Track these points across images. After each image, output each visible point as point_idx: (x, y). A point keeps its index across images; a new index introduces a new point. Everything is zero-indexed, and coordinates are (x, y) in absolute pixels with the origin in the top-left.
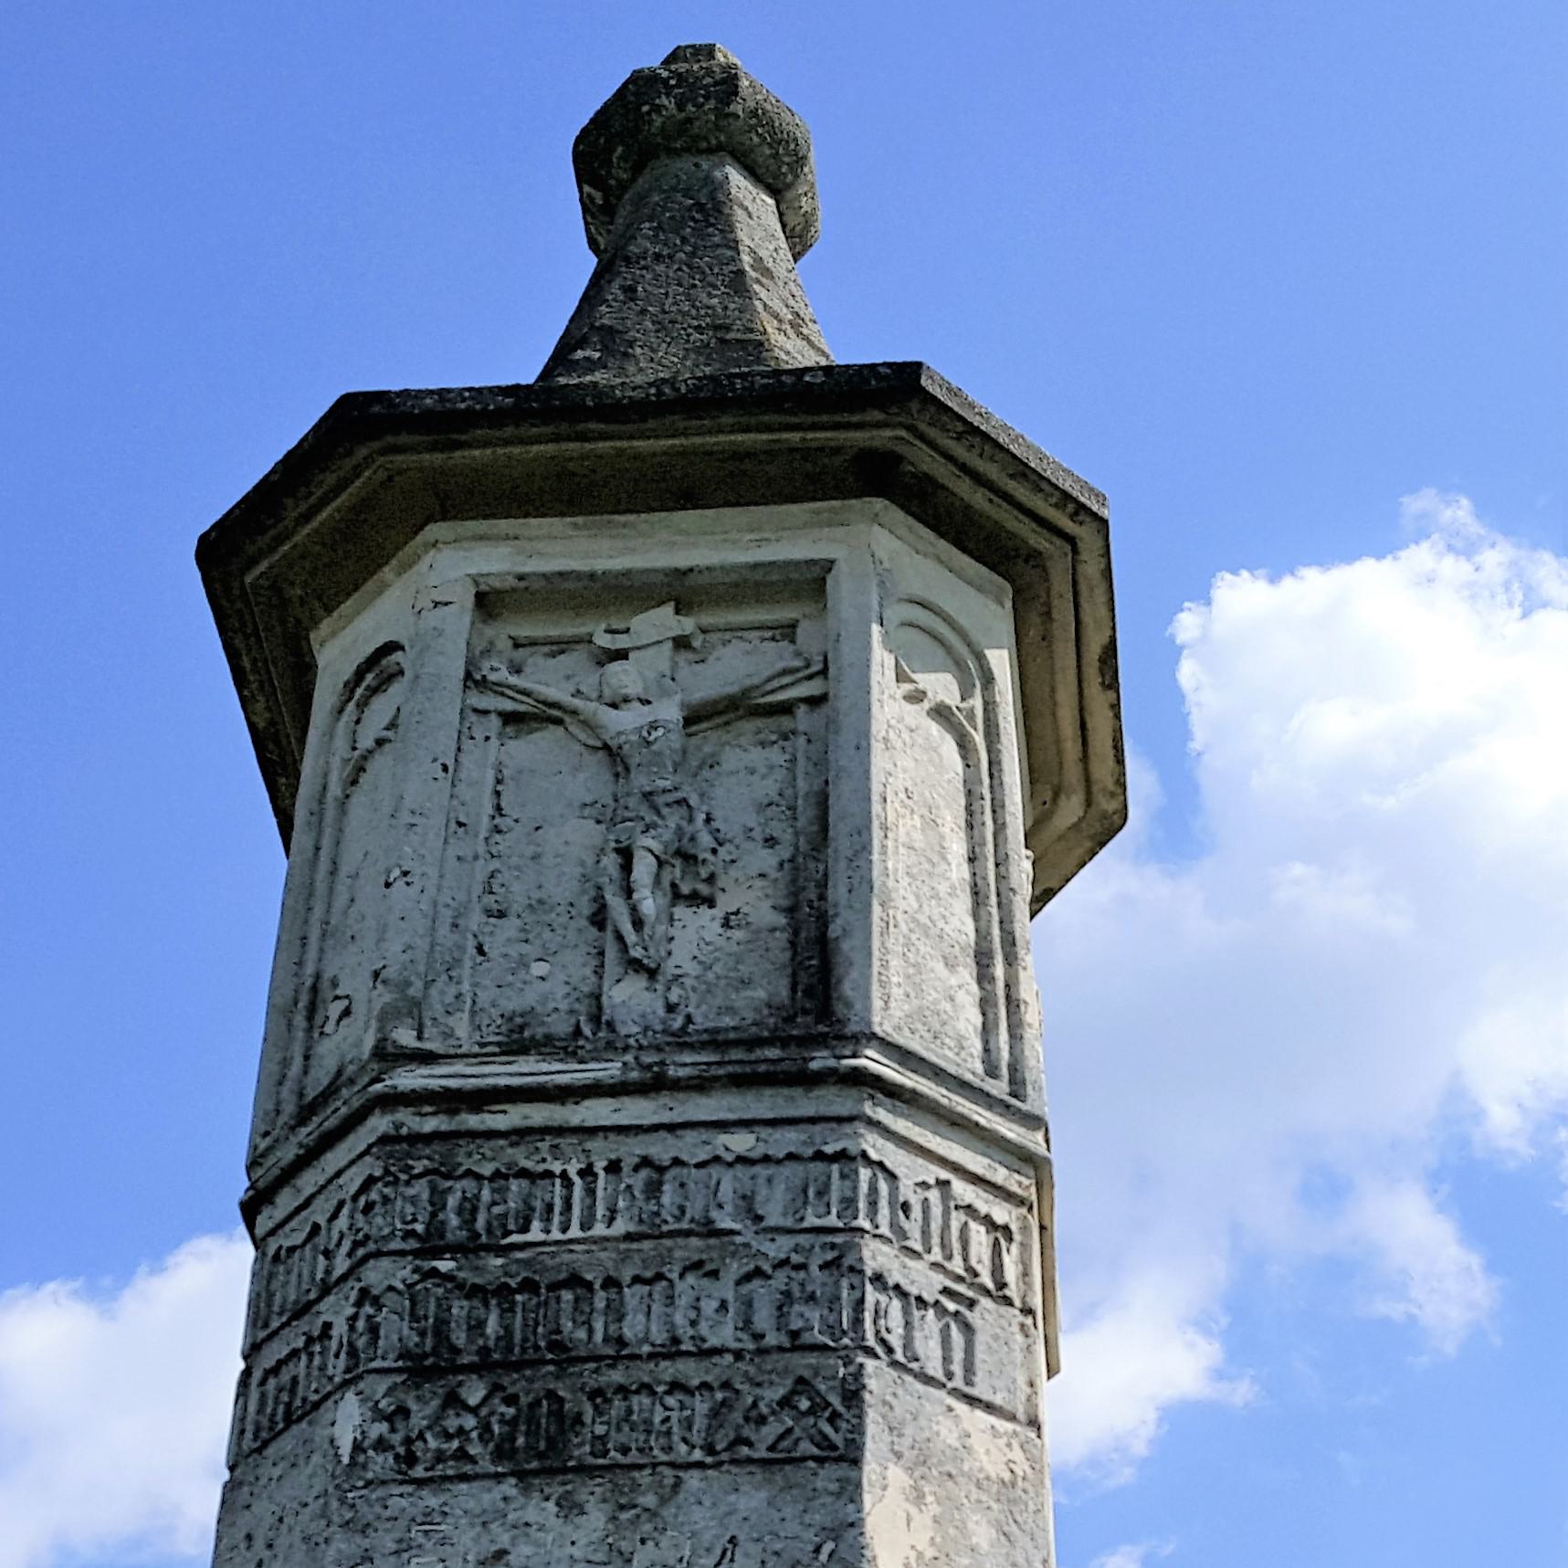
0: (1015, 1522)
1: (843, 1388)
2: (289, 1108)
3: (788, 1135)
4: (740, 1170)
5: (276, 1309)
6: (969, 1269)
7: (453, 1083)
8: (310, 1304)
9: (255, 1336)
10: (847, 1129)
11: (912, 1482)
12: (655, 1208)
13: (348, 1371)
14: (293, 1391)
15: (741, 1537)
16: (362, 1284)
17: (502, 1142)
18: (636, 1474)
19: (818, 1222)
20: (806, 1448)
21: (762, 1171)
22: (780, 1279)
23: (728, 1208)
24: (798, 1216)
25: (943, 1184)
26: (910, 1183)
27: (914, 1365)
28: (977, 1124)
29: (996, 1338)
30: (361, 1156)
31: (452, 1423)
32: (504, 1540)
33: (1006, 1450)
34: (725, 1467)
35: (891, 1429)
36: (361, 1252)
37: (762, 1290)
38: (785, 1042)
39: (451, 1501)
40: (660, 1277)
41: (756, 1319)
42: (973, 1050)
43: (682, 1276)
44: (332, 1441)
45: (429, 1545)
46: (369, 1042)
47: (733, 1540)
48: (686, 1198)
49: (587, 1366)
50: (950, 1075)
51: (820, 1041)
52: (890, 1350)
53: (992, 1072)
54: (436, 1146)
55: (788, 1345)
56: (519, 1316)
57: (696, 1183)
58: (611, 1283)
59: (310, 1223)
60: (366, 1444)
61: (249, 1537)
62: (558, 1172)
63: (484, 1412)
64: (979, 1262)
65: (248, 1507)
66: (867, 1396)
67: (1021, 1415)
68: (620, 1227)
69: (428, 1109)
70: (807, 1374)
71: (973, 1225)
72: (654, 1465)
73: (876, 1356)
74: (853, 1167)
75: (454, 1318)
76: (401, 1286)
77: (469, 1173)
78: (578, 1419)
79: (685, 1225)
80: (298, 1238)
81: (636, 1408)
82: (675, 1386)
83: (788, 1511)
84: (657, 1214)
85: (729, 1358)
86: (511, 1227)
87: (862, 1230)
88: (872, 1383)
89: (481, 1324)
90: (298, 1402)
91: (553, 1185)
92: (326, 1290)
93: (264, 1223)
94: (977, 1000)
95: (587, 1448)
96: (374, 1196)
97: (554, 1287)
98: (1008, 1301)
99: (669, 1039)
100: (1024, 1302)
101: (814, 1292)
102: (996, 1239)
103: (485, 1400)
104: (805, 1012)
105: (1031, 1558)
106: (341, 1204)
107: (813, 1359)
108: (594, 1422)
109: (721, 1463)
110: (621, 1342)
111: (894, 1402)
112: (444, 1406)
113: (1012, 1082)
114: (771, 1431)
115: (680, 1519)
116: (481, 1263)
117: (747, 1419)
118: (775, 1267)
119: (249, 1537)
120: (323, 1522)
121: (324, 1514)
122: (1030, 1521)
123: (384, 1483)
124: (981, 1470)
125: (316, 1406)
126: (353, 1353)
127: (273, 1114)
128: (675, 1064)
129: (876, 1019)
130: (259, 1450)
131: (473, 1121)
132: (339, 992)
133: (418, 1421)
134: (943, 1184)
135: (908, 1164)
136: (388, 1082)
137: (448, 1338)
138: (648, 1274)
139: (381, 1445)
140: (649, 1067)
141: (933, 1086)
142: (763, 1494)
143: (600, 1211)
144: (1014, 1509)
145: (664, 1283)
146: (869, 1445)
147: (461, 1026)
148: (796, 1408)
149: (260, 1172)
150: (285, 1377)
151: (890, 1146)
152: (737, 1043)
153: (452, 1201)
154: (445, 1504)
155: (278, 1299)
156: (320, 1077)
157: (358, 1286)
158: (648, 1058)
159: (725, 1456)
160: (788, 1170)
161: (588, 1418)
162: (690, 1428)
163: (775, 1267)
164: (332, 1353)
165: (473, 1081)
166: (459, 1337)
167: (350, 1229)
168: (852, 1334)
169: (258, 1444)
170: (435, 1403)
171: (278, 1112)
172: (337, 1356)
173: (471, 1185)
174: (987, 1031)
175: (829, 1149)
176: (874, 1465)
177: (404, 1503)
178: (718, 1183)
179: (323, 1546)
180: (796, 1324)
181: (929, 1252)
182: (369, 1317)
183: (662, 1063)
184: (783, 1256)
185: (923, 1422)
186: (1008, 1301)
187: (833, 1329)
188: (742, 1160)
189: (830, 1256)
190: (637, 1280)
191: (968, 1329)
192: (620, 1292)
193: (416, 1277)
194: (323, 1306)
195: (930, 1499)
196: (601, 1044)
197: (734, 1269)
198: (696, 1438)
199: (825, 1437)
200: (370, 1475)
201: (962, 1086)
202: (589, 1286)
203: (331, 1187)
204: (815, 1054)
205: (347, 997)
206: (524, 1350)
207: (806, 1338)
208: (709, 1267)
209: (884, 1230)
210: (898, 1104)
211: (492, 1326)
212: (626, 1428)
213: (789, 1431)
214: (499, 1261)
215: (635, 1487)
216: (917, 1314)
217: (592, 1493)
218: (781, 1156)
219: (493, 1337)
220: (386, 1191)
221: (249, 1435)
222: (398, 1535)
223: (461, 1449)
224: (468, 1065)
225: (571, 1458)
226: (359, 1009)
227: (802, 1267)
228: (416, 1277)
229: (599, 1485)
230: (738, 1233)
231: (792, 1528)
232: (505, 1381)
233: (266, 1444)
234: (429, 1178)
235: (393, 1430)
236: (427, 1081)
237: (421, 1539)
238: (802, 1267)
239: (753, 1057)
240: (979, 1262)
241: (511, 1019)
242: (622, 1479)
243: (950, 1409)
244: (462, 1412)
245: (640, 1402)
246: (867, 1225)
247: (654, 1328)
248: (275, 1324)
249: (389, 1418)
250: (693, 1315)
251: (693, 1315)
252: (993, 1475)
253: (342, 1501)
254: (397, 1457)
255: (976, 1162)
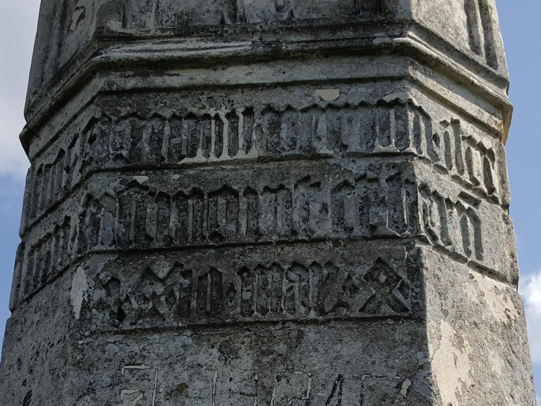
0: (513, 352)
1: (408, 266)
2: (49, 77)
3: (360, 90)
4: (330, 113)
5: (39, 205)
6: (473, 179)
7: (145, 55)
8: (58, 204)
9: (26, 222)
10: (398, 85)
11: (455, 332)
12: (276, 140)
13: (79, 252)
14: (47, 262)
15: (346, 376)
16: (88, 191)
17: (176, 95)
18: (272, 328)
19: (383, 149)
20: (386, 310)
21: (345, 115)
22: (360, 189)
23: (324, 140)
24: (369, 144)
25: (455, 123)
26: (437, 122)
27: (449, 247)
28: (473, 83)
29: (492, 226)
30: (88, 104)
31: (148, 290)
32: (185, 376)
33: (504, 302)
34: (332, 324)
35: (440, 294)
36: (88, 169)
37: (349, 197)
38: (356, 27)
39: (148, 348)
40: (282, 187)
41: (346, 216)
42: (463, 36)
43: (296, 186)
44: (69, 302)
45: (133, 381)
46: (93, 29)
47: (340, 378)
48: (296, 133)
49: (236, 250)
50: (457, 50)
51: (379, 25)
52: (434, 238)
53: (475, 48)
54: (136, 97)
55: (368, 235)
56: (191, 215)
57: (302, 123)
58: (250, 191)
59: (59, 149)
60: (91, 305)
61: (19, 361)
62: (213, 115)
63: (169, 282)
64: (478, 175)
65: (19, 340)
66: (425, 272)
67: (509, 278)
68: (255, 153)
69: (130, 73)
70: (383, 256)
71: (473, 150)
72: (284, 322)
73: (427, 243)
74: (403, 110)
75: (148, 216)
76: (113, 193)
77: (156, 115)
78: (232, 288)
79: (297, 152)
80: (52, 159)
81: (270, 280)
82: (295, 264)
83: (377, 357)
84: (278, 144)
85: (330, 244)
86: (184, 153)
87: (413, 154)
88: (427, 263)
89: (166, 219)
90: (50, 270)
91: (210, 123)
92: (67, 195)
93: (34, 148)
94: (463, 5)
95: (239, 309)
96: (96, 131)
97: (213, 194)
98: (495, 200)
99: (281, 26)
100: (504, 201)
101: (384, 198)
102: (485, 158)
103: (169, 274)
104: (364, 10)
105: (525, 377)
106: (75, 139)
107: (385, 246)
108: (242, 290)
109: (329, 321)
110: (257, 232)
111: (440, 274)
112: (143, 278)
113: (488, 56)
114: (361, 297)
115: (303, 362)
116: (165, 177)
117: (344, 288)
118: (357, 180)
119: (19, 361)
120: (63, 361)
121: (63, 355)
122: (521, 350)
123: (103, 333)
124: (492, 318)
125: (61, 274)
126: (82, 239)
127: (40, 81)
128: (287, 43)
129: (414, 11)
130: (28, 300)
131: (158, 81)
132: (79, 5)
133: (125, 288)
134: (455, 123)
135: (435, 109)
136: (104, 55)
137: (144, 229)
138: (274, 186)
139: (101, 305)
140: (269, 44)
141: (447, 57)
142: (359, 345)
143: (241, 142)
144: (512, 343)
145: (285, 192)
146: (429, 308)
147: (151, 23)
148: (378, 281)
149: (31, 116)
150: (43, 251)
151: (425, 97)
152: (325, 28)
153: (145, 136)
154: (144, 349)
155: (40, 199)
156: (66, 56)
157: (85, 193)
158: (270, 38)
159: (331, 316)
160: (361, 115)
161: (238, 288)
162: (307, 294)
163: (357, 180)
164: (70, 237)
165: (157, 54)
166: (152, 230)
167: (81, 154)
168: (410, 227)
169: (27, 296)
170: (137, 276)
171: (42, 79)
172: (73, 240)
173: (156, 124)
174: (470, 24)
175: (388, 99)
176: (432, 322)
177: (117, 349)
178: (317, 124)
179: (62, 378)
180: (374, 221)
181: (451, 169)
182: (93, 214)
183: (278, 41)
184: (362, 173)
185: (457, 288)
186: (495, 200)
187: (397, 223)
188: (331, 106)
189: (392, 173)
190: (267, 189)
191: (476, 220)
192: (257, 198)
193: (123, 187)
194: (65, 205)
195: (466, 342)
196: (238, 30)
197: (330, 182)
198: (312, 303)
199: (397, 301)
200: (94, 328)
201: (463, 58)
202: (236, 194)
203: (71, 126)
204: (376, 35)
205: (83, 7)
206: (194, 238)
207: (381, 230)
208: (313, 181)
209: (425, 154)
210: (427, 69)
211: (173, 221)
212: (264, 296)
213: (373, 297)
214: (177, 177)
215: (272, 338)
216: (448, 211)
217: (243, 343)
218: (356, 103)
219: (174, 229)
220: (103, 128)
221: (22, 289)
222: (113, 372)
223: (154, 308)
224: (154, 44)
225: (228, 317)
226: (88, 13)
227: (376, 180)
228: (123, 187)
229: (249, 336)
230: (331, 157)
231: (380, 369)
232: (183, 261)
233: (31, 296)
234: (131, 119)
235: (109, 294)
236: (128, 54)
237: (128, 376)
238: (376, 180)
239: (335, 37)
240: (478, 175)
241: (180, 17)
242: (262, 331)
243: (472, 277)
244: (155, 283)
245: (273, 275)
246: (414, 151)
247: (280, 224)
248: (38, 216)
249: (106, 286)
250: (304, 214)
251: (304, 214)
252: (499, 321)
253: (75, 346)
254: (112, 313)
255: (472, 109)
